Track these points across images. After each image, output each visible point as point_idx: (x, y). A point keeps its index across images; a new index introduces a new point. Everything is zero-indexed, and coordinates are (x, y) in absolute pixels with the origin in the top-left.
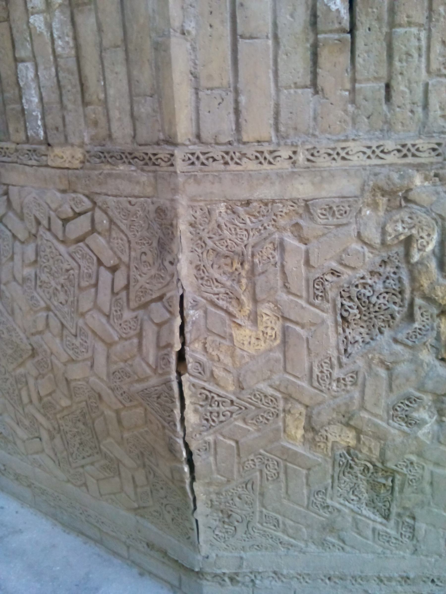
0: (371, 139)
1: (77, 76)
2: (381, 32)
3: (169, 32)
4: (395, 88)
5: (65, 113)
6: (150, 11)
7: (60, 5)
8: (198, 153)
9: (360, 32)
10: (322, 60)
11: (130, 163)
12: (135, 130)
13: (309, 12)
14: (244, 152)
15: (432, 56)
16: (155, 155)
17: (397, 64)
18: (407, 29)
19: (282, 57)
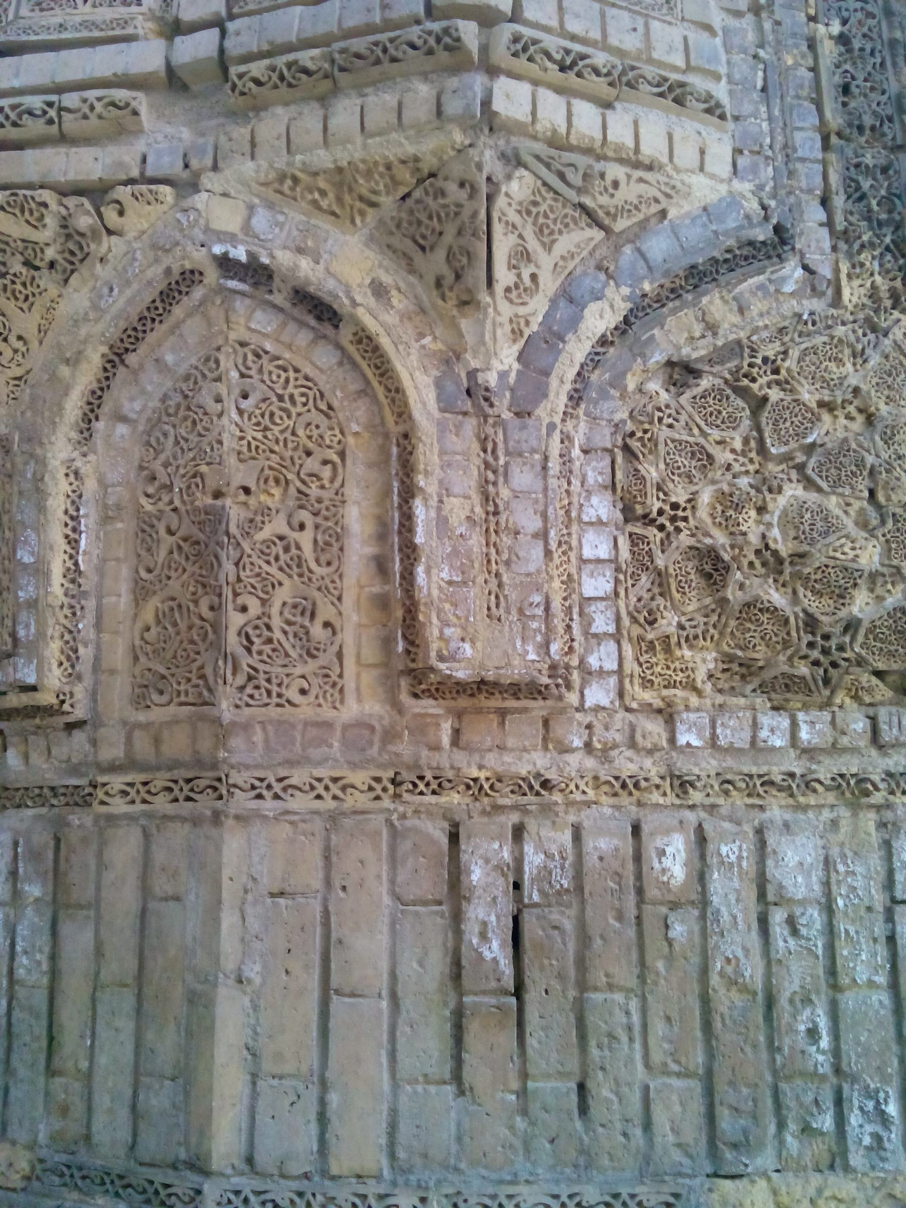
0: (557, 1182)
1: (44, 1023)
2: (566, 998)
3: (217, 977)
4: (594, 1093)
5: (11, 1084)
6: (189, 939)
7: (37, 900)
8: (247, 1192)
9: (532, 996)
10: (469, 1039)
11: (117, 1194)
12: (135, 1135)
13: (448, 960)
14: (331, 1194)
15: (652, 1041)
16: (166, 1186)
17: (594, 1052)
18: (608, 995)
19: (403, 1029)
